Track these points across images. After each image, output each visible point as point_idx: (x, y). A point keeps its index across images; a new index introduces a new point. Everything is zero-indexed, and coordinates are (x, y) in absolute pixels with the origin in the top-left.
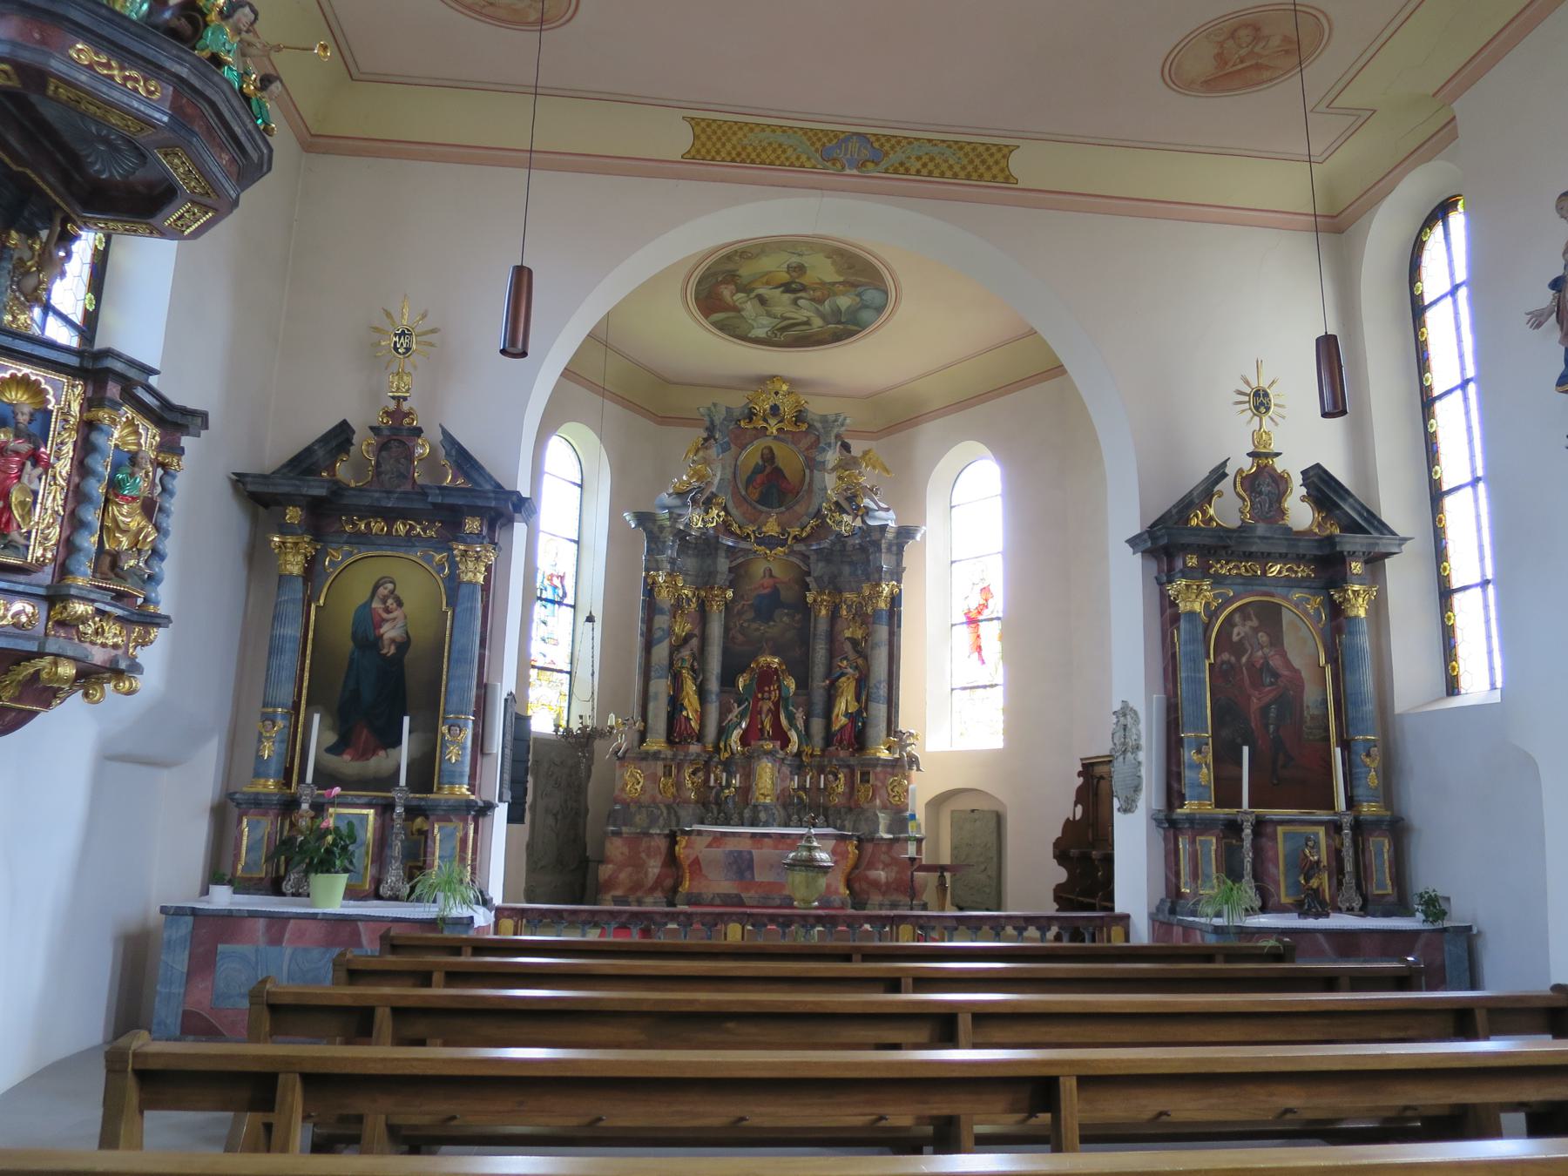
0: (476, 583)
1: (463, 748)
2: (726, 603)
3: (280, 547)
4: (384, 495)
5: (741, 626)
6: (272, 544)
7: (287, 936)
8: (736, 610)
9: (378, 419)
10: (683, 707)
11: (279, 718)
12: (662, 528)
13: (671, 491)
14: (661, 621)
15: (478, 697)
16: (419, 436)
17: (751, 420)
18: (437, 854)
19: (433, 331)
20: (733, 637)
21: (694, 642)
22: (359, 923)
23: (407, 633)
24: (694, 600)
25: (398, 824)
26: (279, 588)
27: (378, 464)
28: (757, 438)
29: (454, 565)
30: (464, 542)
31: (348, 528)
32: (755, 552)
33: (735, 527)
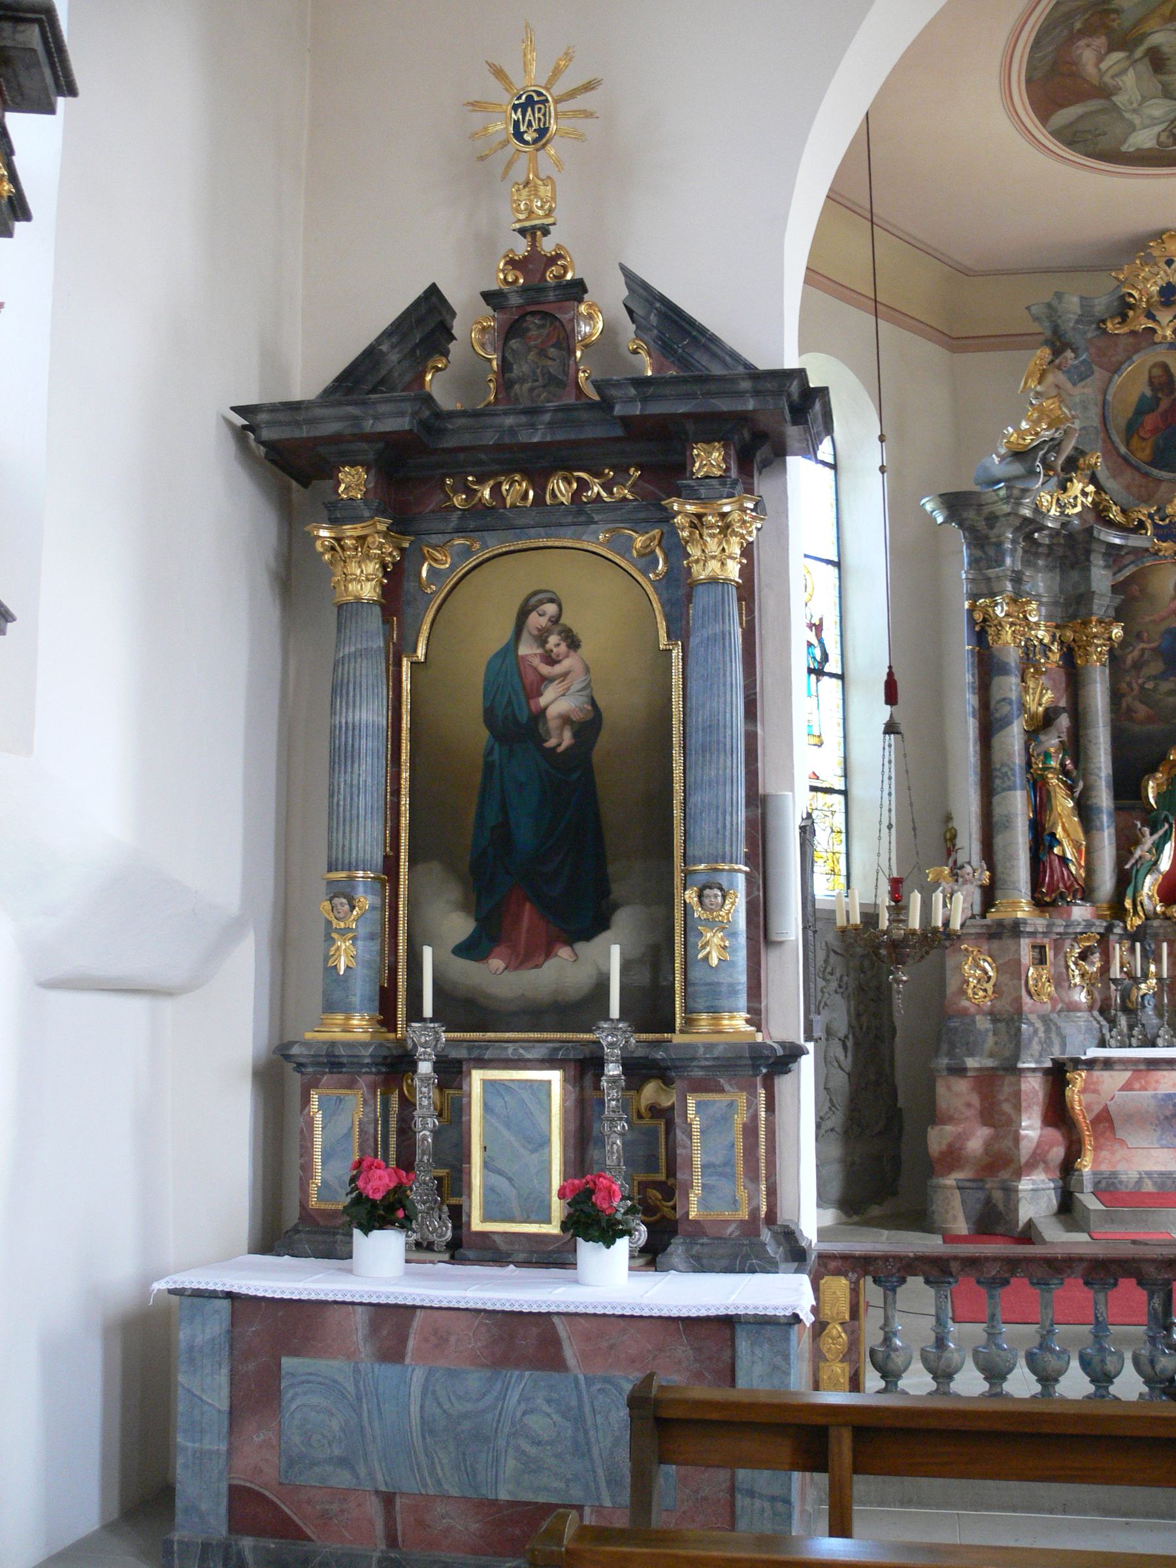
0: (727, 582)
1: (733, 935)
2: (1111, 651)
3: (333, 548)
4: (523, 419)
5: (1142, 687)
6: (318, 544)
7: (411, 1344)
8: (1129, 661)
9: (497, 277)
10: (1054, 840)
11: (361, 889)
12: (992, 520)
13: (1003, 451)
14: (1009, 686)
15: (750, 823)
16: (580, 301)
17: (1124, 318)
18: (697, 1161)
19: (588, 87)
20: (1130, 710)
21: (1064, 721)
22: (556, 1320)
23: (593, 703)
24: (1055, 648)
25: (612, 1097)
26: (339, 630)
27: (505, 366)
28: (1136, 351)
29: (676, 550)
30: (691, 495)
31: (459, 500)
32: (1156, 553)
33: (1115, 514)
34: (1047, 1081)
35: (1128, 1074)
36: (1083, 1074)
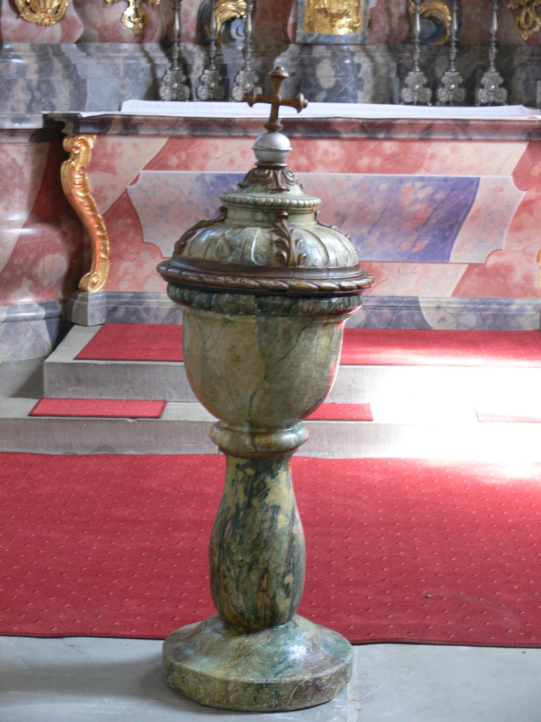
34: (38, 151)
35: (160, 143)
36: (91, 142)
